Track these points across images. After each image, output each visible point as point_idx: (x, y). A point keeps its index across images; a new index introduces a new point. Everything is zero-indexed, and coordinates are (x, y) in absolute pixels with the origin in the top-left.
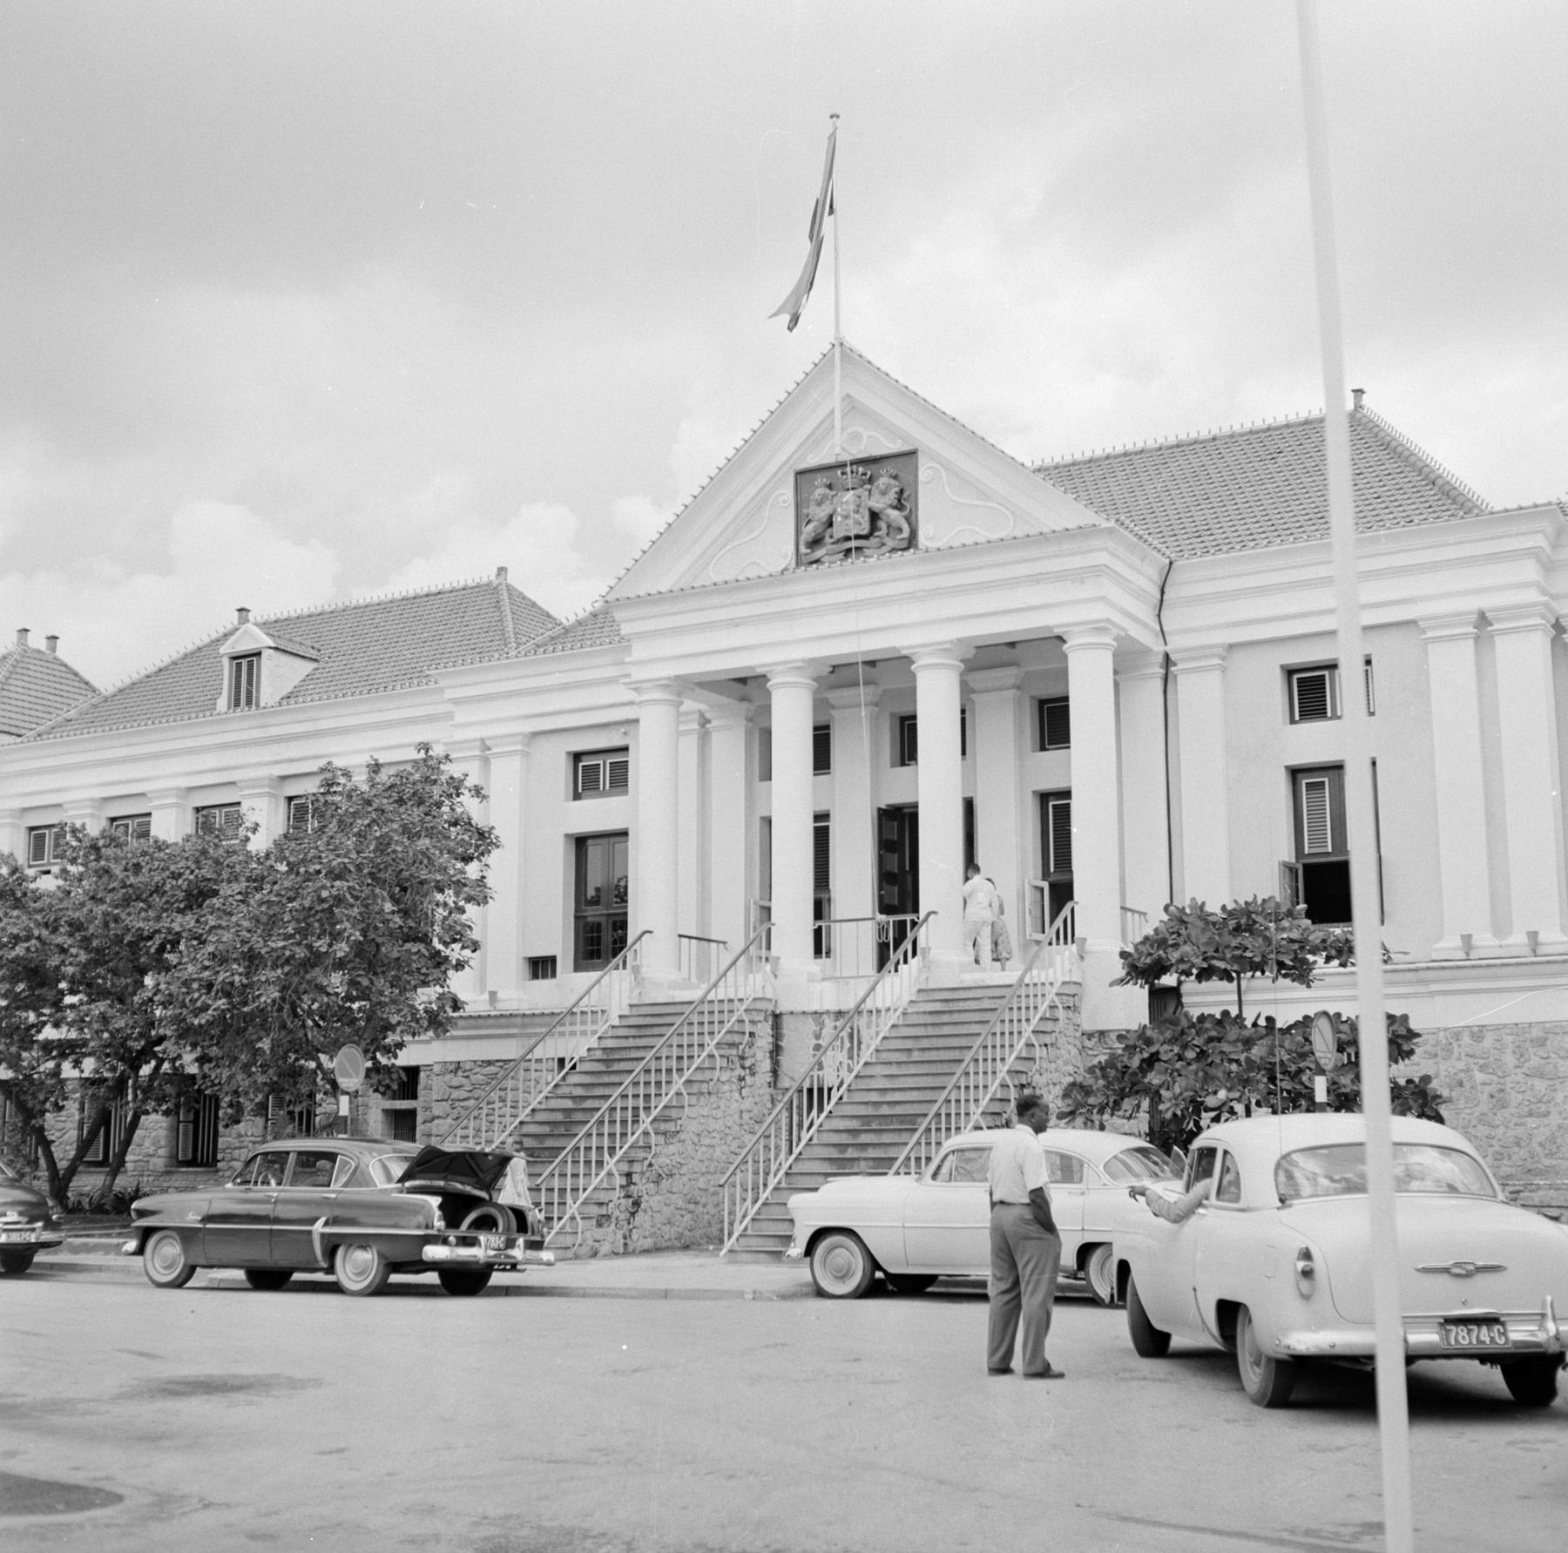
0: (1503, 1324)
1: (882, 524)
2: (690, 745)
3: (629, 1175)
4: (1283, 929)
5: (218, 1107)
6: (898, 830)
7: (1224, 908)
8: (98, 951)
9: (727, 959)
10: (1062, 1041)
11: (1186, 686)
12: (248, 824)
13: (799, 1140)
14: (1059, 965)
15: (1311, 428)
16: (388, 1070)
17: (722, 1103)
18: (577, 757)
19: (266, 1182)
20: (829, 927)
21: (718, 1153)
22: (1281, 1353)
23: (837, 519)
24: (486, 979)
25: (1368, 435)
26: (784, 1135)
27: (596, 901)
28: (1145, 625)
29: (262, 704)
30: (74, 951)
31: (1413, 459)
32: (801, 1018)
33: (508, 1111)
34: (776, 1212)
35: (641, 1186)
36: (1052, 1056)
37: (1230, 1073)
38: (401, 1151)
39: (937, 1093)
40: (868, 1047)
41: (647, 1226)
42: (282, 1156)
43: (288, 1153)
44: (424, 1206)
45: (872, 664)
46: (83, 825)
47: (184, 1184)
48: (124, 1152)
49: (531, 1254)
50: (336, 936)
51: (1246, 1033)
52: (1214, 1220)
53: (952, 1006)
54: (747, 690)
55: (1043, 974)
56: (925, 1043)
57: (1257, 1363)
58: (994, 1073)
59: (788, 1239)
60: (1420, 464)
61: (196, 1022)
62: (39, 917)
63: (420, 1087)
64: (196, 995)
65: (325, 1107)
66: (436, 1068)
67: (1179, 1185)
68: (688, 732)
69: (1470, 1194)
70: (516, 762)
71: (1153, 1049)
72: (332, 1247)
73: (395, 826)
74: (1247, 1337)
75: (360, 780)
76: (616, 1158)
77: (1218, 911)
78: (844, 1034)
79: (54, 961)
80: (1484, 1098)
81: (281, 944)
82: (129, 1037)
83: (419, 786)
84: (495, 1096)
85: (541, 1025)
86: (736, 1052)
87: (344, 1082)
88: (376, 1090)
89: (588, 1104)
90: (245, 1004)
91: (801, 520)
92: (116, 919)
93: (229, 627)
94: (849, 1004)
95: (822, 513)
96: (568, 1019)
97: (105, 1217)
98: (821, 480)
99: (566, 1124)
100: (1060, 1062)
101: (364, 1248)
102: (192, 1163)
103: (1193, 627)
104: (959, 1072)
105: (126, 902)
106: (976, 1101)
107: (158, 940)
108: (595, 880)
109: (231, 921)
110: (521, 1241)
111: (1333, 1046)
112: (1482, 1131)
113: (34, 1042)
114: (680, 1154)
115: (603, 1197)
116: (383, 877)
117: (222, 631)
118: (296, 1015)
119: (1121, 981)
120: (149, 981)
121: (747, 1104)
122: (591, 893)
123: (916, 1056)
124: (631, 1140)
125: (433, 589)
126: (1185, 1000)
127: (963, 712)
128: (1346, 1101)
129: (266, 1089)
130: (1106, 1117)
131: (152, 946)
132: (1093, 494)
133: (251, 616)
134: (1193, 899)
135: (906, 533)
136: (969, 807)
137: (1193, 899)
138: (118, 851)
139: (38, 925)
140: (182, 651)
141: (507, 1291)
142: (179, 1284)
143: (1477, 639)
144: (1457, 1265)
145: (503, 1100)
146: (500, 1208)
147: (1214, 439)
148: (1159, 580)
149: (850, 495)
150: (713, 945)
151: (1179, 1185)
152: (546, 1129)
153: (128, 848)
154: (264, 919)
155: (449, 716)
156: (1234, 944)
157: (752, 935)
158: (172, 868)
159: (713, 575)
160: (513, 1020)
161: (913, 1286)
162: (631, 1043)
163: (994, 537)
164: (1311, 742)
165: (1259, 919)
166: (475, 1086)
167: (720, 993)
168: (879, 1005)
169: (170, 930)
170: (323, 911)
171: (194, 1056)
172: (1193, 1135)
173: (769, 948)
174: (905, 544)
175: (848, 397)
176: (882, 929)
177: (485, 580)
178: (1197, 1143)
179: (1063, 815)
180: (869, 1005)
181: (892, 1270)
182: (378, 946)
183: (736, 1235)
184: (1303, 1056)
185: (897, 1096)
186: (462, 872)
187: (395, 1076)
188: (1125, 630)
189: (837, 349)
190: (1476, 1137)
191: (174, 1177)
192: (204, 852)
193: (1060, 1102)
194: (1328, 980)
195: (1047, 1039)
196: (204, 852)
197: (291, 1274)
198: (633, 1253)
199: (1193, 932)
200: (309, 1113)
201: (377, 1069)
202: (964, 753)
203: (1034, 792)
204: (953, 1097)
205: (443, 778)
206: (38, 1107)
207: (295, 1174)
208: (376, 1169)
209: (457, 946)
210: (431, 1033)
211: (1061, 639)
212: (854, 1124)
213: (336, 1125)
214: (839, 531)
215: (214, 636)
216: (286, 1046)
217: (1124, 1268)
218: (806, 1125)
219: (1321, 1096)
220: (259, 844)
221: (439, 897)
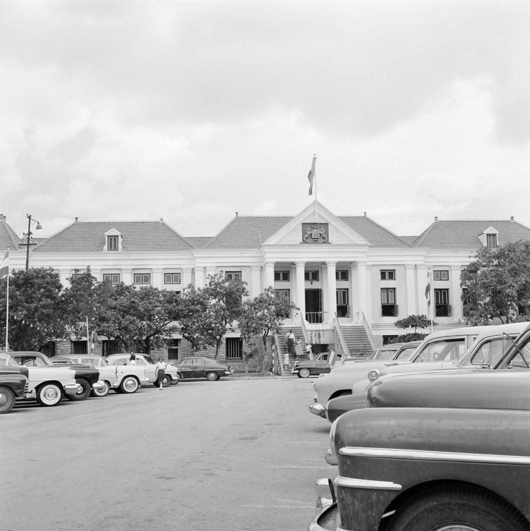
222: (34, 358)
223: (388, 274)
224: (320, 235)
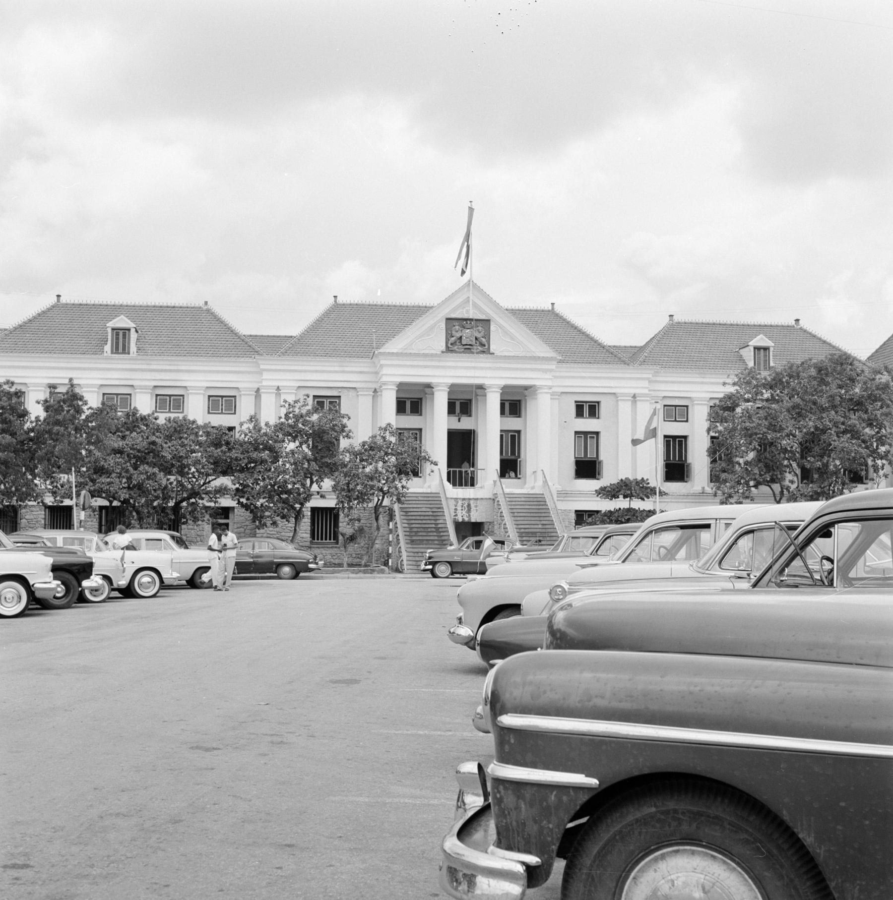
220: (598, 782)
223: (587, 409)
224: (476, 339)
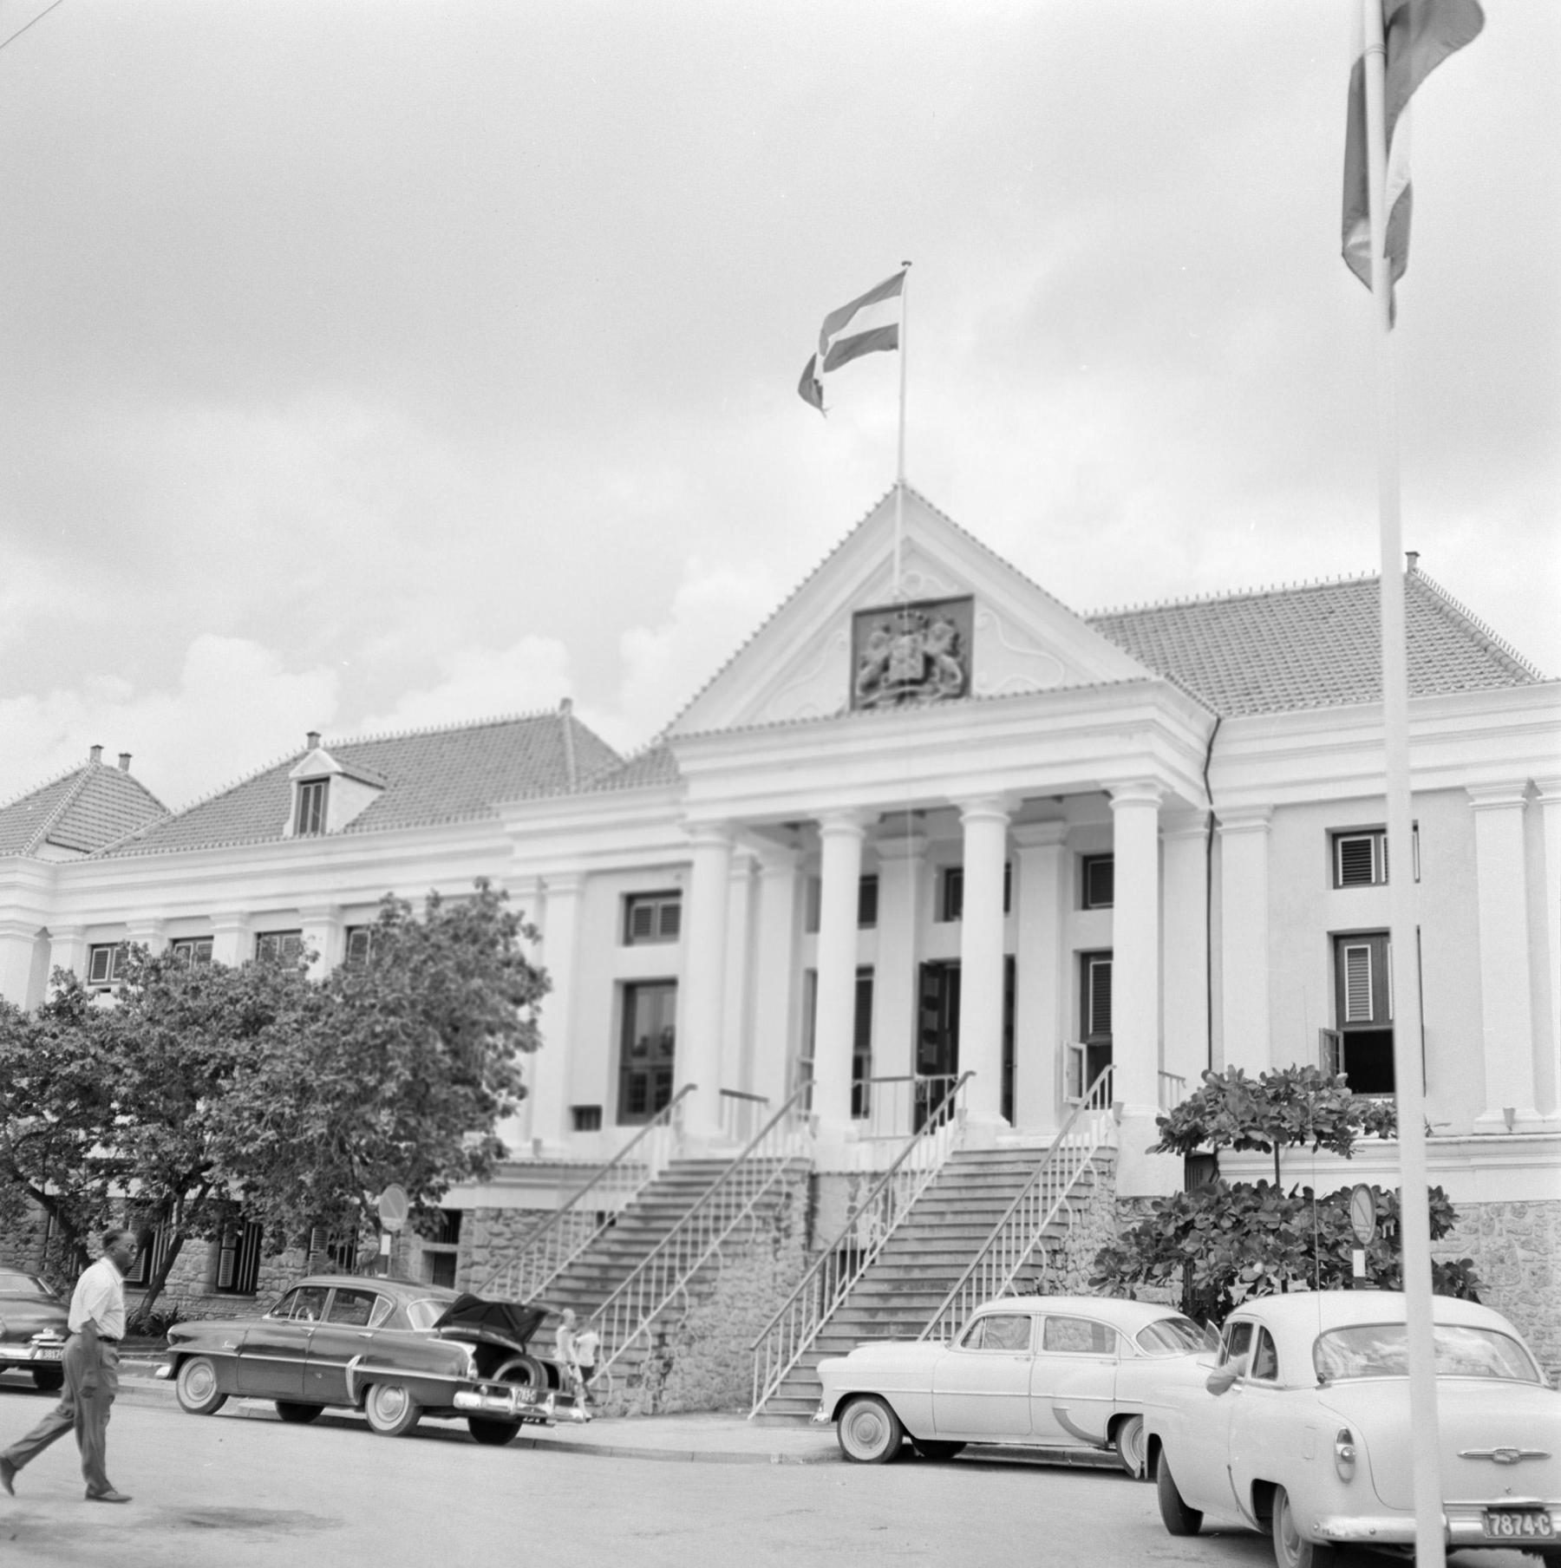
0: (1547, 1513)
1: (936, 670)
2: (740, 891)
3: (661, 1336)
4: (1322, 1099)
5: (260, 1236)
6: (939, 986)
7: (1263, 1075)
8: (152, 1073)
9: (767, 1117)
10: (1096, 1206)
11: (1229, 846)
12: (308, 953)
13: (831, 1303)
14: (1095, 1129)
15: (1364, 590)
16: (431, 1212)
17: (757, 1266)
18: (630, 899)
19: (303, 1316)
20: (868, 1087)
21: (750, 1316)
22: (1320, 1538)
23: (893, 663)
24: (531, 1128)
25: (1424, 601)
26: (816, 1299)
27: (641, 1052)
28: (1195, 786)
29: (328, 831)
30: (128, 1071)
31: (1465, 624)
32: (837, 1180)
33: (546, 1263)
34: (804, 1376)
35: (674, 1348)
36: (1085, 1223)
37: (1266, 1246)
38: (439, 1296)
39: (998, 1216)
40: (902, 1209)
41: (678, 1387)
42: (322, 1291)
43: (327, 1289)
44: (460, 1353)
45: (920, 813)
46: (146, 946)
47: (222, 1310)
48: (164, 1275)
49: (561, 1410)
50: (387, 1074)
51: (1284, 1204)
52: (1252, 1396)
53: (985, 1169)
54: (798, 834)
55: (1079, 1138)
56: (958, 1206)
57: (1294, 1547)
58: (1027, 1238)
59: (816, 1403)
60: (1473, 630)
61: (244, 1151)
62: (96, 1036)
63: (462, 1231)
64: (246, 1124)
65: (367, 1244)
66: (479, 1214)
67: (1212, 1358)
68: (738, 878)
69: (1509, 1379)
70: (570, 903)
71: (1188, 1218)
72: (365, 1386)
73: (450, 963)
74: (1283, 1521)
75: (419, 914)
76: (650, 1318)
77: (1257, 1079)
78: (879, 1196)
79: (108, 1081)
80: (1525, 1275)
81: (332, 1077)
82: (177, 1161)
83: (475, 923)
84: (534, 1246)
85: (585, 1178)
86: (773, 1216)
87: (387, 1222)
88: (418, 1232)
89: (625, 1261)
90: (294, 1135)
91: (858, 662)
92: (172, 1042)
93: (299, 751)
94: (885, 1166)
95: (877, 656)
96: (609, 1174)
97: (141, 1339)
98: (879, 621)
99: (602, 1281)
100: (1093, 1228)
101: (396, 1389)
102: (230, 1290)
103: (1243, 784)
104: (992, 1236)
105: (184, 1025)
106: (1008, 1266)
107: (212, 1065)
108: (642, 1028)
109: (284, 1059)
110: (551, 1396)
111: (1371, 1220)
112: (1524, 1309)
113: (81, 1160)
114: (713, 1316)
115: (635, 1356)
116: (437, 1009)
117: (292, 754)
118: (342, 1150)
119: (1159, 1149)
120: (200, 1106)
121: (781, 1266)
122: (637, 1042)
123: (949, 1219)
124: (665, 1300)
125: (499, 720)
126: (1222, 1168)
127: (1008, 866)
128: (1387, 1277)
129: (310, 1222)
130: (1139, 1284)
131: (207, 1070)
132: (1144, 647)
133: (321, 741)
134: (1231, 1066)
135: (959, 680)
136: (1010, 965)
137: (1231, 1066)
138: (179, 975)
139: (94, 1042)
140: (252, 774)
141: (534, 1444)
142: (210, 1410)
143: (1526, 809)
144: (1500, 1452)
145: (541, 1251)
146: (534, 1362)
147: (1266, 596)
148: (1206, 737)
149: (906, 640)
150: (755, 1104)
151: (1212, 1358)
152: (581, 1285)
153: (189, 971)
154: (317, 1051)
155: (507, 851)
156: (1274, 1111)
157: (793, 1093)
158: (231, 993)
159: (772, 715)
160: (555, 1171)
161: (941, 1453)
162: (670, 1200)
163: (1045, 686)
164: (1357, 908)
165: (1298, 1088)
166: (515, 1235)
167: (759, 1153)
168: (915, 1166)
169: (224, 1055)
170: (375, 1046)
171: (240, 1183)
172: (1228, 1307)
173: (809, 1106)
174: (956, 691)
175: (907, 540)
176: (920, 1090)
177: (549, 712)
178: (1232, 1318)
179: (1102, 978)
180: (904, 1167)
181: (920, 1436)
182: (428, 1086)
183: (764, 1398)
184: (1341, 1228)
185: (929, 1260)
186: (513, 1015)
187: (437, 1219)
188: (1171, 787)
189: (900, 491)
190: (1517, 1315)
191: (212, 1303)
192: (263, 979)
193: (1092, 1269)
194: (1368, 1151)
195: (1081, 1205)
196: (263, 979)
197: (321, 1408)
198: (663, 1414)
199: (1231, 1101)
200: (350, 1249)
201: (419, 1210)
202: (1007, 908)
203: (1076, 952)
204: (985, 1262)
205: (500, 915)
206: (82, 1225)
207: (334, 1308)
208: (416, 1311)
209: (504, 1092)
210: (474, 1178)
211: (1107, 794)
212: (884, 1288)
213: (376, 1263)
214: (894, 675)
215: (284, 759)
216: (332, 1180)
217: (1155, 1442)
218: (838, 1287)
219: (1359, 1270)
220: (317, 973)
221: (489, 1039)
222: (721, 1125)
